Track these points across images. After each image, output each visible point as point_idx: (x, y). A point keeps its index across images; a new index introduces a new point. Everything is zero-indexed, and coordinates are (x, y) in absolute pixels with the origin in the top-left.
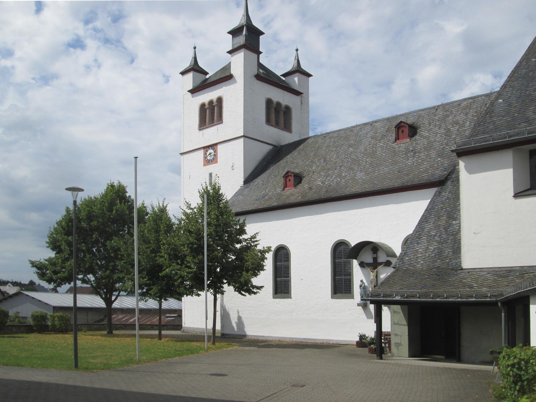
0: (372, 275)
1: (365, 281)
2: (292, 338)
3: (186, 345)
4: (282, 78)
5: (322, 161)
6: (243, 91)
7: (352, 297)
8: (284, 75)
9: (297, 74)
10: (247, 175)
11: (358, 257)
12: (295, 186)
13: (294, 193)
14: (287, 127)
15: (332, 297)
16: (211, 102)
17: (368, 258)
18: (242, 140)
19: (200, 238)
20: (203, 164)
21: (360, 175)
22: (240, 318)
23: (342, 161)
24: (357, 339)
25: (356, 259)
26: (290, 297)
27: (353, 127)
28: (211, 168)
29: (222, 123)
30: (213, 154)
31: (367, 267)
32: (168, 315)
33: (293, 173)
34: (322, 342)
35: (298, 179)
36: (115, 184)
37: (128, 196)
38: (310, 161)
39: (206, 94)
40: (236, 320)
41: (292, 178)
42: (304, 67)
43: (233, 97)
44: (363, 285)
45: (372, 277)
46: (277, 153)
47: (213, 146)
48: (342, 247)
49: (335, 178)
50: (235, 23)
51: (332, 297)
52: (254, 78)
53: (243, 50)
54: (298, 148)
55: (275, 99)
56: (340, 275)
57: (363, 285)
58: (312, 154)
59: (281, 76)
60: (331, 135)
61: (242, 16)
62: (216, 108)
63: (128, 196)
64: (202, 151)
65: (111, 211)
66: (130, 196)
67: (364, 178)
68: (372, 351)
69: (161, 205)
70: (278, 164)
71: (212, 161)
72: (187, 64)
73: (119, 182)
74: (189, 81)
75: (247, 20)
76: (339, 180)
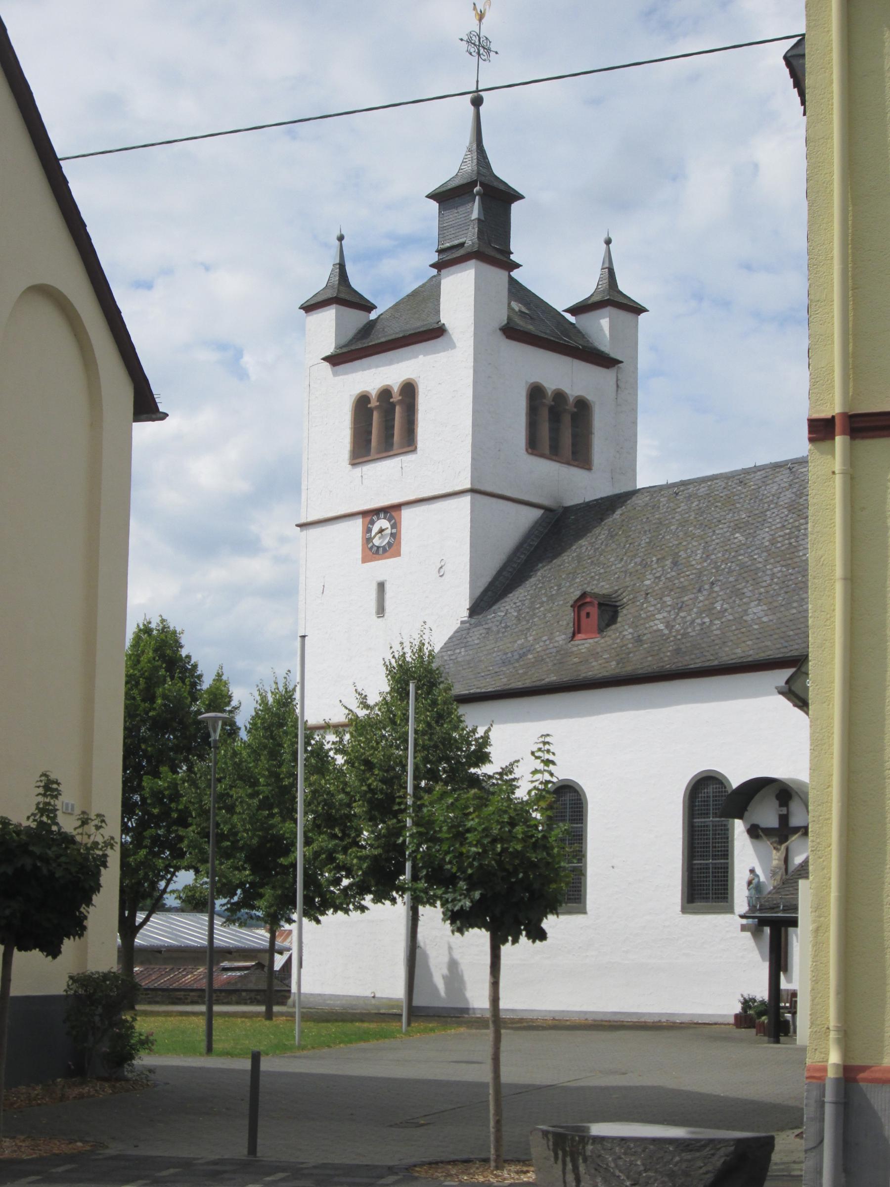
0: (776, 858)
1: (759, 871)
2: (586, 1013)
3: (349, 1027)
4: (568, 316)
5: (668, 563)
6: (471, 371)
7: (730, 910)
8: (575, 310)
9: (608, 310)
10: (478, 592)
11: (746, 814)
12: (601, 630)
13: (597, 651)
14: (580, 455)
15: (684, 910)
16: (385, 393)
17: (769, 817)
18: (467, 499)
19: (394, 780)
20: (360, 556)
21: (756, 610)
22: (453, 965)
23: (717, 568)
24: (738, 1009)
25: (741, 817)
26: (583, 911)
27: (746, 472)
28: (382, 568)
29: (414, 450)
30: (388, 531)
31: (765, 838)
32: (226, 964)
33: (595, 596)
34: (656, 1019)
35: (608, 610)
36: (153, 625)
37: (184, 656)
38: (638, 560)
39: (373, 370)
40: (445, 971)
41: (594, 611)
42: (627, 286)
43: (447, 382)
44: (755, 882)
45: (775, 863)
46: (556, 531)
47: (391, 511)
48: (710, 790)
49: (700, 613)
51: (684, 910)
52: (500, 333)
53: (473, 262)
54: (609, 521)
55: (551, 385)
56: (703, 857)
57: (755, 882)
58: (645, 539)
59: (564, 311)
60: (691, 489)
61: (464, 151)
62: (398, 409)
63: (184, 656)
64: (358, 524)
65: (152, 699)
66: (188, 657)
67: (765, 619)
68: (763, 1030)
69: (281, 688)
70: (556, 562)
71: (385, 551)
72: (318, 278)
73: (163, 621)
74: (326, 329)
75: (478, 164)
76: (707, 620)
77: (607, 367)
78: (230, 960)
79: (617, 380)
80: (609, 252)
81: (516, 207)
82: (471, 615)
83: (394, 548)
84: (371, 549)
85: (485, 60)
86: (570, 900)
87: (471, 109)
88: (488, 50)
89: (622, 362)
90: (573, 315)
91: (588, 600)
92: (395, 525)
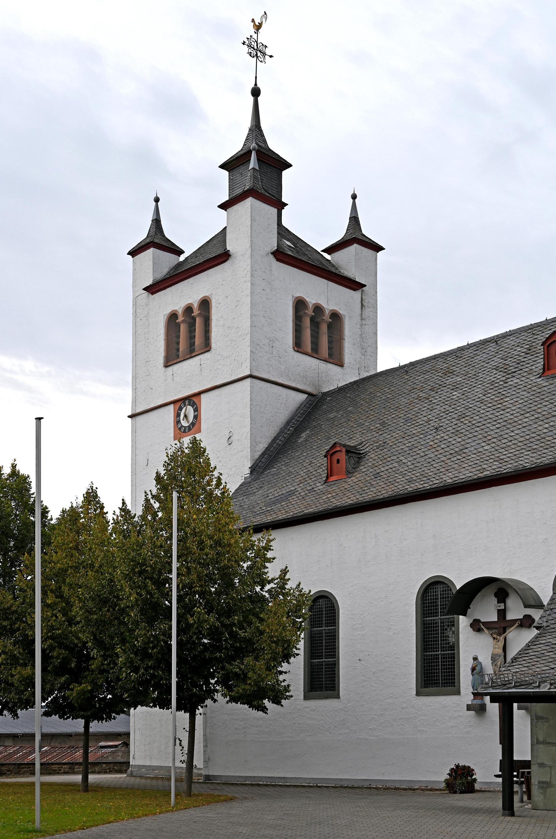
16: (189, 309)
25: (465, 614)
32: (102, 744)
41: (342, 456)
42: (368, 230)
44: (478, 668)
47: (192, 400)
48: (439, 589)
50: (235, 145)
59: (323, 251)
77: (355, 290)
78: (106, 741)
79: (362, 300)
80: (354, 206)
81: (286, 174)
82: (251, 473)
83: (196, 426)
84: (180, 429)
85: (261, 62)
86: (327, 689)
87: (252, 99)
88: (264, 54)
89: (365, 286)
90: (329, 254)
91: (338, 449)
92: (197, 410)
